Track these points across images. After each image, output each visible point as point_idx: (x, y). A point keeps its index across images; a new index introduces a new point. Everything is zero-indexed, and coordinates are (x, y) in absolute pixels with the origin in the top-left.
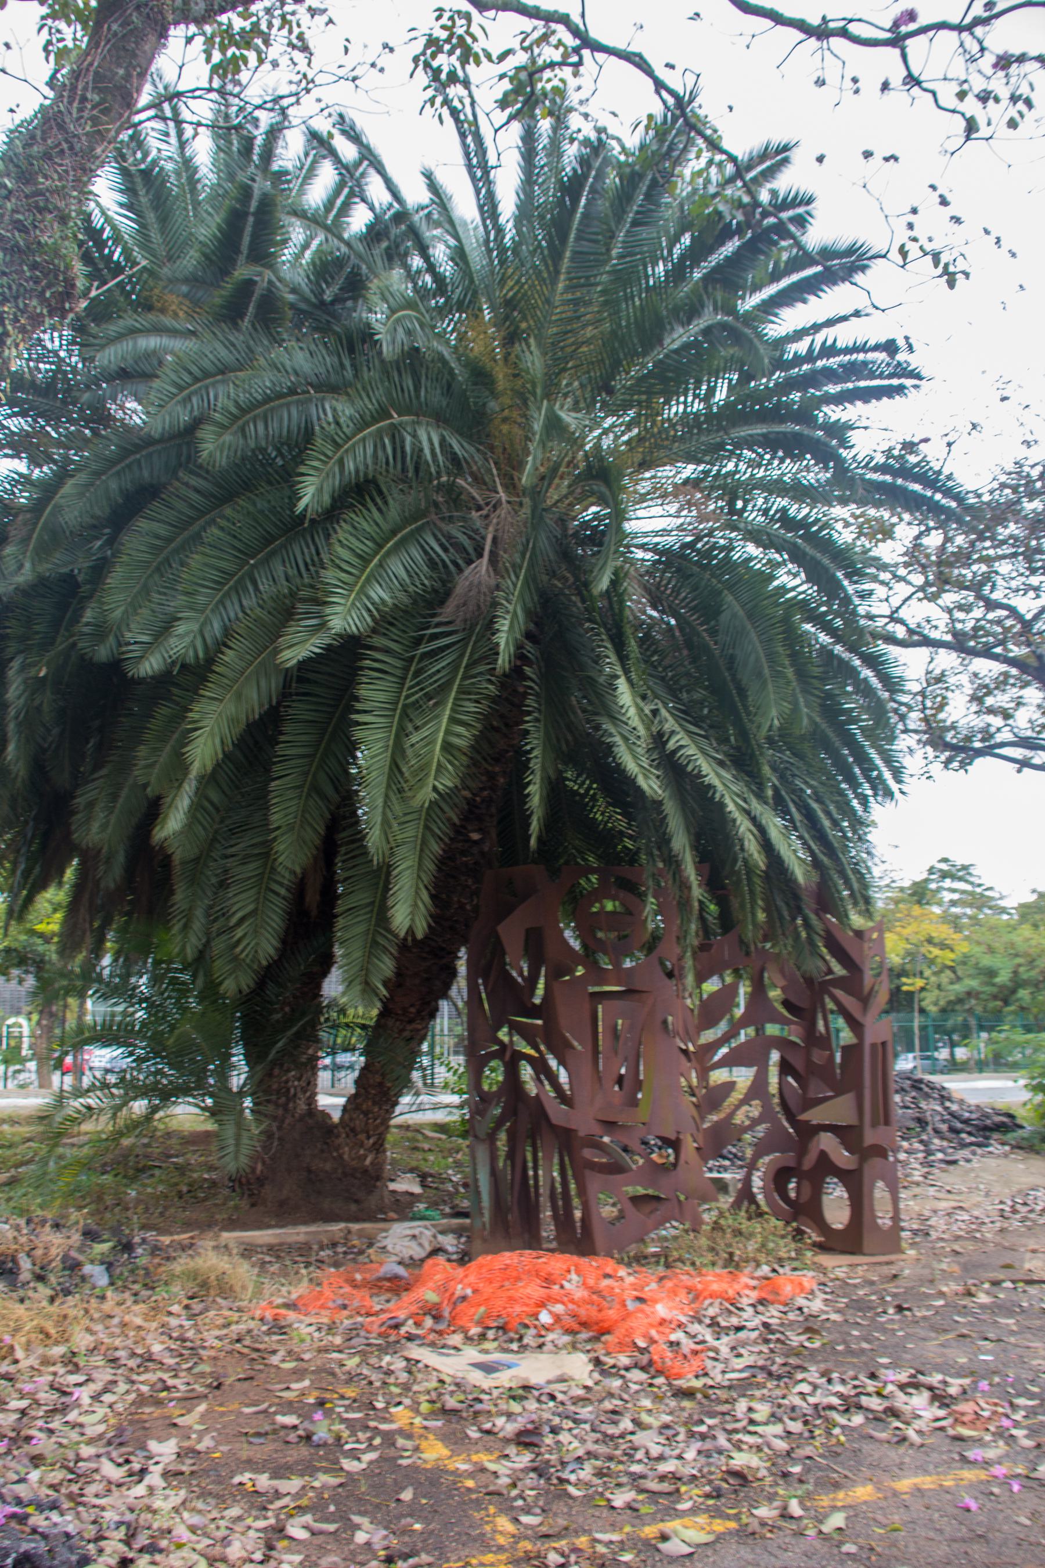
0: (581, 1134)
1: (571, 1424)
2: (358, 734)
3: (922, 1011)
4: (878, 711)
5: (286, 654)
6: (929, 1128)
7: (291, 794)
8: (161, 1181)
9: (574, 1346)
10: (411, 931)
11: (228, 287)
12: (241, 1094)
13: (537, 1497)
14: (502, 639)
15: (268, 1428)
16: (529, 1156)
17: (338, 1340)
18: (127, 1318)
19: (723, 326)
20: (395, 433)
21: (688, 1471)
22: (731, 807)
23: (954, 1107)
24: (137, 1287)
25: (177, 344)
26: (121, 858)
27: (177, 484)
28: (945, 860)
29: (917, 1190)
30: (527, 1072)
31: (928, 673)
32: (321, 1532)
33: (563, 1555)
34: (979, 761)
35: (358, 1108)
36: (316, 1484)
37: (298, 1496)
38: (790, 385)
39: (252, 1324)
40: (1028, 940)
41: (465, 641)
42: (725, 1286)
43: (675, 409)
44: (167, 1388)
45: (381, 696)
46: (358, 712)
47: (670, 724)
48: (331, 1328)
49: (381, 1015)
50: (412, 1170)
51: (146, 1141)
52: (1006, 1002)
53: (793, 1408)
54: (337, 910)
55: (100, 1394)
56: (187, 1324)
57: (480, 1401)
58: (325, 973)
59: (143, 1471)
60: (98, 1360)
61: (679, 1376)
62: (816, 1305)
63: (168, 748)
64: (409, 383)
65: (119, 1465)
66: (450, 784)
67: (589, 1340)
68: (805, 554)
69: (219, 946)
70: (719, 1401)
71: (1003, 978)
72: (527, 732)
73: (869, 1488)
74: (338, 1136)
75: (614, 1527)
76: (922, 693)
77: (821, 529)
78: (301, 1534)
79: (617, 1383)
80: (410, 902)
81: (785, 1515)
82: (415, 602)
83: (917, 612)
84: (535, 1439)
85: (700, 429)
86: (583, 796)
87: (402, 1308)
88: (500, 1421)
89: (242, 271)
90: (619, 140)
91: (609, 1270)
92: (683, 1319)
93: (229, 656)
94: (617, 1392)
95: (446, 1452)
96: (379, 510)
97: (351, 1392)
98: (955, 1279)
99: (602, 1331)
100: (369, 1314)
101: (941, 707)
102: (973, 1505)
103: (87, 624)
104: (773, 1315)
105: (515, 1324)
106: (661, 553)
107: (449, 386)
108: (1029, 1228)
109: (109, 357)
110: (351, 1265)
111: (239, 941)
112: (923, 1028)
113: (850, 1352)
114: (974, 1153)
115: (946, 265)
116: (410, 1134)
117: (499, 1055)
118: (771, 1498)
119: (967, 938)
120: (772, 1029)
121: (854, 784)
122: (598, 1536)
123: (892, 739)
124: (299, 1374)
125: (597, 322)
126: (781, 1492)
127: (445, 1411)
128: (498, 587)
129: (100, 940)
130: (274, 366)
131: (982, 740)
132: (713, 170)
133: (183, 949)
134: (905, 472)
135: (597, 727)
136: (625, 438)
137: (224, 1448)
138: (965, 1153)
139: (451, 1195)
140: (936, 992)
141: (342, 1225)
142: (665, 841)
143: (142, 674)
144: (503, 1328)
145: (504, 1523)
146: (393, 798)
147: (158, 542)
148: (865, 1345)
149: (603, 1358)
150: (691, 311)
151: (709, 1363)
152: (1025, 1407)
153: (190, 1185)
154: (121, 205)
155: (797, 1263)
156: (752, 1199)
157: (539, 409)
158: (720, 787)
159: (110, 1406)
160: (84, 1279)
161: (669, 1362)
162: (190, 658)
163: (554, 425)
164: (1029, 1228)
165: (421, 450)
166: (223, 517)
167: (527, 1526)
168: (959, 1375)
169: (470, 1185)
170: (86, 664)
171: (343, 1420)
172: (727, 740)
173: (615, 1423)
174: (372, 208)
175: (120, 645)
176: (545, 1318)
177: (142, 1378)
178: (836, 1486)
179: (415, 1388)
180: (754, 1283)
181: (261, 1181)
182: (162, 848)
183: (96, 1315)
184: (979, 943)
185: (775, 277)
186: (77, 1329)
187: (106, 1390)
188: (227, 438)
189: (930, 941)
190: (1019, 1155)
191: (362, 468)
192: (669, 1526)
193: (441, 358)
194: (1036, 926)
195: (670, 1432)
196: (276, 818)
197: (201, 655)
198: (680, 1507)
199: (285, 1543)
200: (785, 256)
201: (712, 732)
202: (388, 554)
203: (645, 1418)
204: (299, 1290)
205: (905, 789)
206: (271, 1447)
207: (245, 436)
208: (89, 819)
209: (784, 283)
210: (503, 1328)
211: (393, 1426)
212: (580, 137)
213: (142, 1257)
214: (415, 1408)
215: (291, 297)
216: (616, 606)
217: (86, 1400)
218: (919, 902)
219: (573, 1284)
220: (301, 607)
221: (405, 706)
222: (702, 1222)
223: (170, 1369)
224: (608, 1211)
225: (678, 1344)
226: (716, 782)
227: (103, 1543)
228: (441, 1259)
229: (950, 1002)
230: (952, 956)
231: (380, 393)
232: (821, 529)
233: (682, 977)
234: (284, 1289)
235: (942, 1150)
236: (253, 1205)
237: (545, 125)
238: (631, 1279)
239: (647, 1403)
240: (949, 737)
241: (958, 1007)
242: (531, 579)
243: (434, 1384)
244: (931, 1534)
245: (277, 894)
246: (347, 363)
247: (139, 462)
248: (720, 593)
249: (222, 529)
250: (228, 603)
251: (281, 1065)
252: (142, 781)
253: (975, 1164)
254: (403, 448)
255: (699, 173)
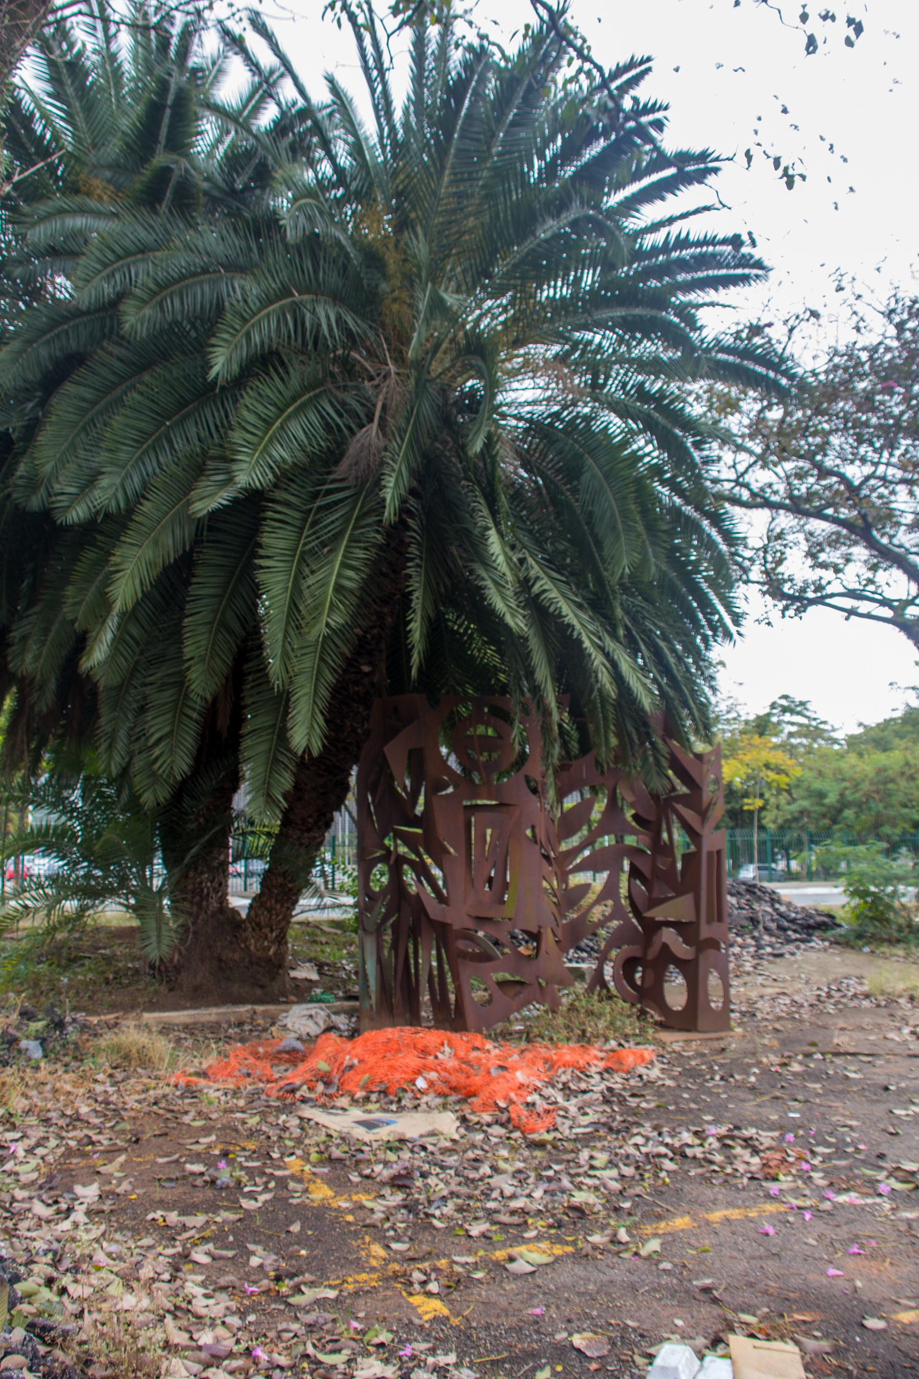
0: (456, 927)
1: (438, 1170)
2: (261, 576)
3: (762, 828)
4: (719, 563)
5: (197, 506)
6: (761, 927)
7: (202, 629)
8: (90, 970)
9: (445, 1106)
10: (307, 750)
11: (147, 173)
12: (161, 893)
13: (406, 1229)
14: (389, 494)
15: (178, 1174)
16: (411, 950)
17: (242, 1103)
18: (58, 1085)
19: (589, 219)
20: (296, 309)
21: (535, 1206)
22: (587, 644)
23: (783, 909)
24: (67, 1059)
25: (102, 225)
26: (52, 685)
27: (100, 352)
28: (785, 697)
29: (747, 978)
30: (409, 877)
31: (770, 530)
32: (221, 1258)
33: (425, 1274)
34: (812, 609)
35: (262, 905)
36: (219, 1219)
37: (202, 1229)
38: (646, 274)
39: (167, 1090)
40: (853, 767)
41: (356, 495)
42: (577, 1057)
43: (546, 293)
44: (92, 1143)
45: (282, 544)
46: (262, 557)
47: (535, 570)
48: (236, 1093)
49: (283, 825)
50: (310, 961)
51: (77, 935)
52: (834, 821)
53: (628, 1156)
54: (244, 731)
55: (33, 1148)
56: (111, 1090)
57: (362, 1151)
58: (235, 788)
59: (70, 1210)
60: (32, 1120)
61: (533, 1131)
62: (655, 1073)
63: (93, 588)
64: (308, 264)
65: (49, 1205)
66: (341, 621)
67: (459, 1102)
68: (657, 424)
69: (138, 763)
70: (565, 1151)
71: (832, 799)
72: (410, 576)
73: (687, 1219)
74: (245, 930)
75: (470, 1251)
76: (765, 549)
77: (672, 402)
78: (204, 1259)
79: (480, 1137)
80: (307, 724)
81: (614, 1240)
82: (312, 461)
83: (759, 477)
84: (407, 1182)
85: (567, 312)
86: (462, 635)
87: (297, 1075)
88: (378, 1168)
89: (161, 159)
90: (499, 47)
91: (478, 1044)
92: (539, 1084)
93: (147, 507)
94: (479, 1144)
95: (330, 1193)
96: (282, 379)
97: (251, 1145)
98: (775, 1053)
99: (468, 1094)
100: (269, 1081)
101: (780, 562)
102: (771, 1231)
103: (21, 477)
104: (616, 1081)
105: (394, 1088)
106: (530, 421)
107: (345, 268)
108: (840, 1010)
109: (39, 234)
110: (255, 1041)
111: (157, 759)
112: (762, 843)
113: (680, 1111)
114: (798, 948)
115: (786, 169)
116: (309, 930)
117: (384, 859)
118: (603, 1228)
119: (801, 765)
120: (630, 840)
121: (697, 626)
122: (456, 1258)
123: (730, 585)
124: (206, 1131)
125: (478, 214)
126: (612, 1222)
127: (330, 1160)
128: (386, 449)
129: (37, 759)
130: (188, 247)
131: (815, 591)
132: (582, 77)
133: (109, 765)
134: (747, 353)
135: (472, 572)
136: (501, 319)
137: (140, 1191)
138: (791, 947)
139: (344, 982)
140: (775, 812)
141: (248, 1007)
142: (530, 673)
143: (70, 521)
144: (385, 1092)
145: (377, 1250)
146: (290, 630)
147: (84, 405)
148: (693, 1106)
149: (469, 1116)
150: (559, 205)
151: (559, 1120)
152: (823, 1155)
153: (116, 973)
154: (49, 95)
155: (641, 1038)
156: (604, 985)
157: (424, 291)
158: (578, 626)
159: (43, 1158)
160: (20, 1051)
161: (524, 1120)
162: (113, 507)
163: (437, 305)
164: (840, 1010)
165: (319, 325)
166: (142, 383)
167: (396, 1252)
168: (770, 1129)
169: (361, 973)
170: (20, 513)
171: (242, 1168)
172: (587, 586)
173: (477, 1169)
174: (279, 104)
175: (50, 495)
176: (421, 1083)
177: (71, 1135)
178: (659, 1217)
179: (307, 1141)
180: (602, 1055)
181: (178, 969)
182: (88, 676)
183: (31, 1083)
184: (810, 769)
185: (637, 176)
186: (14, 1094)
187: (38, 1145)
188: (147, 311)
189: (767, 766)
190: (836, 950)
191: (266, 341)
192: (515, 1251)
193: (338, 243)
194: (861, 755)
195: (522, 1176)
196: (189, 650)
197: (122, 505)
198: (526, 1235)
199: (190, 1266)
200: (647, 158)
201: (572, 579)
202: (289, 417)
203: (502, 1165)
204: (210, 1061)
205: (741, 630)
206: (181, 1190)
207: (162, 311)
208: (23, 651)
209: (646, 181)
210: (385, 1092)
211: (287, 1173)
212: (465, 43)
213: (72, 1033)
214: (306, 1158)
215: (205, 185)
216: (489, 467)
217: (21, 1153)
218: (761, 734)
219: (446, 1055)
220: (211, 464)
221: (302, 553)
222: (560, 1004)
223: (95, 1127)
224: (479, 995)
225: (534, 1104)
226: (575, 622)
227: (32, 1266)
228: (333, 1035)
229: (786, 821)
230: (786, 780)
231: (284, 276)
232: (672, 402)
233: (545, 793)
234: (196, 1061)
235: (771, 945)
236: (171, 990)
237: (433, 31)
238: (497, 1051)
239: (504, 1153)
240: (786, 588)
241: (794, 825)
242: (415, 441)
243: (323, 1138)
244: (735, 1254)
245: (190, 718)
246: (254, 246)
247: (67, 332)
248: (582, 456)
249: (141, 394)
250: (147, 461)
251: (196, 869)
252: (70, 617)
253: (799, 957)
254: (303, 323)
255: (570, 81)
